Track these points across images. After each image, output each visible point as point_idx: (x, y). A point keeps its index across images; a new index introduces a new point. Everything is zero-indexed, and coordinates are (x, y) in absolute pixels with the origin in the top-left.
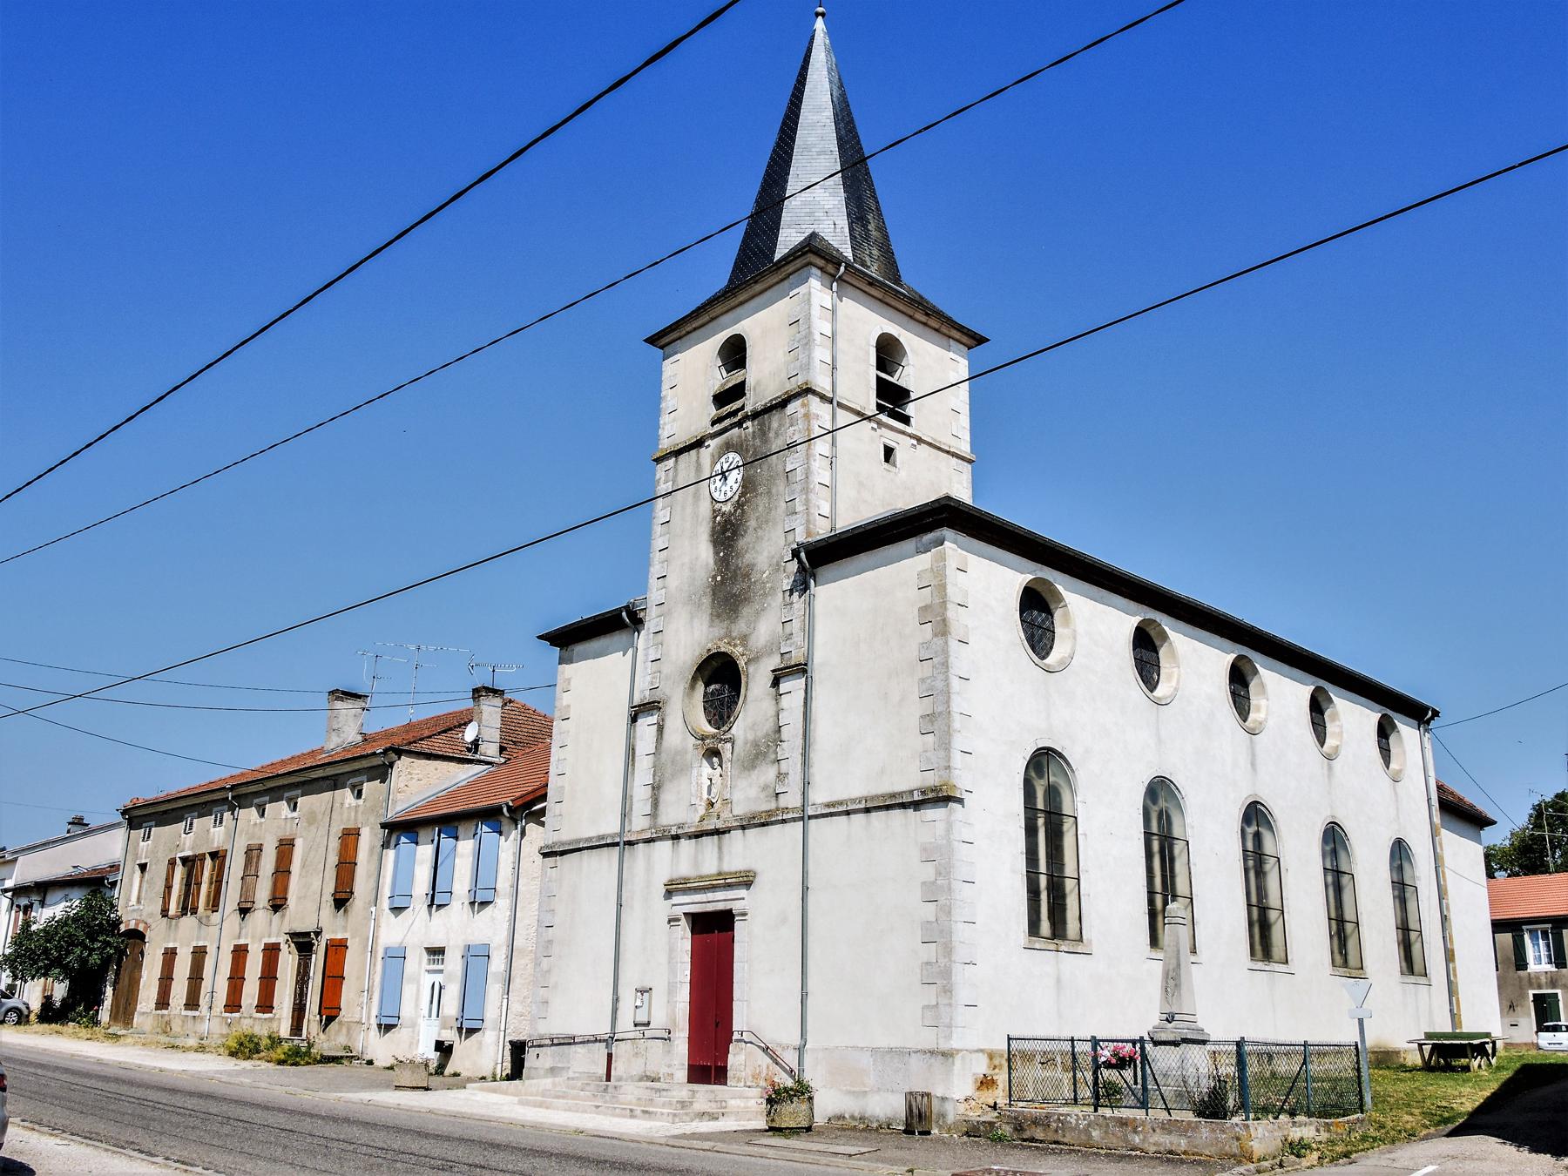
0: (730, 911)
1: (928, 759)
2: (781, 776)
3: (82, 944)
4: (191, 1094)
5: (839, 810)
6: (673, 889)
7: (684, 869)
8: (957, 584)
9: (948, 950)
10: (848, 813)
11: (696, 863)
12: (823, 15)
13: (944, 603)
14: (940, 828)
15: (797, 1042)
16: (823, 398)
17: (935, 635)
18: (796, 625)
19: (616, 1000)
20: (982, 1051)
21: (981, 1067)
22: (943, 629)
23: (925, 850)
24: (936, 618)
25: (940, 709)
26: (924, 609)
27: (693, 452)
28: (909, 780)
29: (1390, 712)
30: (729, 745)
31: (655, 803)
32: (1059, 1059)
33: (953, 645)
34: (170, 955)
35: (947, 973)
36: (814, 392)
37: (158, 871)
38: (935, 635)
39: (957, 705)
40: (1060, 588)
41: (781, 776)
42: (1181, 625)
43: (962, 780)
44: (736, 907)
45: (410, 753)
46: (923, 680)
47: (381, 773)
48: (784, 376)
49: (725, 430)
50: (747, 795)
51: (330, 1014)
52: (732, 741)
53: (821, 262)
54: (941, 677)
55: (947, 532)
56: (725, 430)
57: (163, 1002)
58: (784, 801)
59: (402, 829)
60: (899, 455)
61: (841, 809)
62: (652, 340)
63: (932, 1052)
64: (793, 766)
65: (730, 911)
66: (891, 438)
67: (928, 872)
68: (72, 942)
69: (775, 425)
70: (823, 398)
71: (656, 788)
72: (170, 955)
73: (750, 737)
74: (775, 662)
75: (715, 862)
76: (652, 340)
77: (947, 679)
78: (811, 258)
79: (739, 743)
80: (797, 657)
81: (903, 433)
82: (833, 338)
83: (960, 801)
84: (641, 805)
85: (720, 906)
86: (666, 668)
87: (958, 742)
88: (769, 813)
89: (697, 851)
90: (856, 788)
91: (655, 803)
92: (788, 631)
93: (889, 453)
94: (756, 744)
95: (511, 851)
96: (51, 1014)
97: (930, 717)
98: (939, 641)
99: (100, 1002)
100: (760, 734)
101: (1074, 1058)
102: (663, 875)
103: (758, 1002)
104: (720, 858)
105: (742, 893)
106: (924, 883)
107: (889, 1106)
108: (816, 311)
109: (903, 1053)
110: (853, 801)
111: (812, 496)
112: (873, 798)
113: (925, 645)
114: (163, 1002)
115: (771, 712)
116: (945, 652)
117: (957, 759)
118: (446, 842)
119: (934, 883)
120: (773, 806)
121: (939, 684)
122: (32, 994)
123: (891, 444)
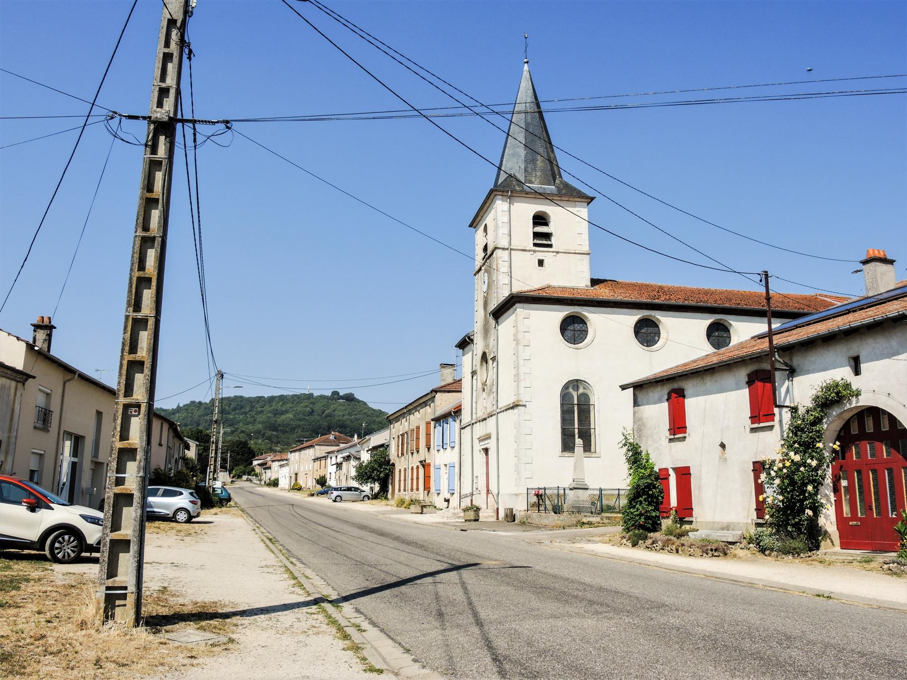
3: (376, 469)
4: (319, 513)
12: (527, 62)
34: (400, 471)
37: (396, 439)
40: (585, 313)
42: (665, 313)
45: (440, 391)
47: (433, 399)
51: (897, 505)
55: (517, 305)
57: (399, 490)
59: (440, 419)
60: (545, 263)
62: (471, 226)
66: (540, 256)
68: (373, 469)
72: (400, 471)
76: (471, 226)
93: (541, 263)
95: (453, 426)
96: (376, 497)
99: (387, 492)
105: (488, 441)
114: (399, 490)
118: (445, 425)
122: (366, 488)
123: (541, 258)
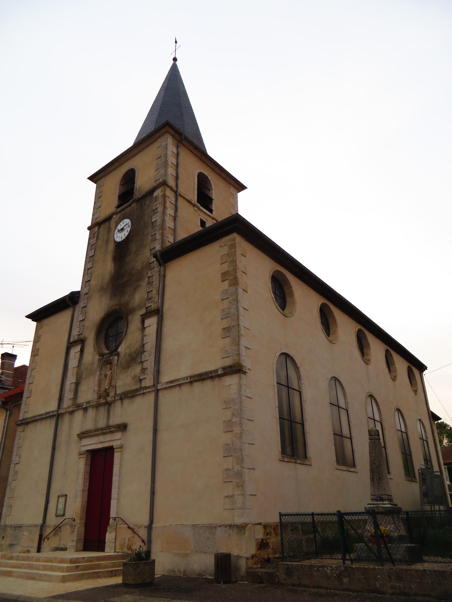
0: (113, 446)
1: (226, 351)
2: (143, 370)
5: (175, 384)
6: (83, 435)
7: (89, 426)
8: (241, 262)
9: (241, 461)
10: (180, 385)
11: (96, 420)
13: (235, 270)
14: (234, 388)
15: (147, 523)
16: (171, 189)
17: (230, 286)
18: (154, 292)
19: (47, 502)
20: (260, 524)
21: (260, 534)
22: (235, 282)
23: (225, 402)
24: (231, 277)
25: (233, 323)
26: (224, 274)
27: (107, 224)
28: (216, 363)
29: (410, 365)
30: (116, 357)
31: (76, 392)
32: (300, 527)
33: (240, 291)
35: (240, 475)
36: (168, 186)
38: (230, 286)
39: (243, 322)
41: (143, 370)
43: (247, 363)
44: (115, 444)
46: (223, 310)
48: (153, 181)
49: (123, 210)
50: (124, 382)
52: (118, 355)
53: (173, 132)
54: (234, 306)
56: (123, 210)
58: (144, 384)
61: (176, 383)
63: (230, 526)
64: (150, 364)
65: (113, 446)
67: (228, 415)
69: (148, 203)
70: (171, 189)
71: (77, 384)
73: (128, 352)
74: (143, 311)
75: (105, 421)
77: (237, 308)
78: (167, 128)
79: (122, 355)
80: (154, 306)
81: (210, 216)
82: (177, 166)
83: (245, 373)
84: (68, 395)
85: (107, 445)
86: (86, 323)
87: (244, 342)
88: (137, 390)
89: (96, 415)
90: (185, 371)
91: (76, 392)
92: (150, 296)
94: (130, 355)
97: (227, 330)
98: (233, 289)
100: (133, 350)
101: (314, 526)
102: (77, 430)
103: (128, 500)
104: (108, 418)
105: (118, 435)
106: (224, 421)
107: (203, 563)
108: (169, 153)
109: (212, 528)
110: (183, 379)
111: (165, 232)
112: (194, 376)
113: (225, 292)
115: (140, 338)
116: (236, 294)
117: (243, 351)
119: (230, 421)
120: (138, 386)
121: (233, 311)
